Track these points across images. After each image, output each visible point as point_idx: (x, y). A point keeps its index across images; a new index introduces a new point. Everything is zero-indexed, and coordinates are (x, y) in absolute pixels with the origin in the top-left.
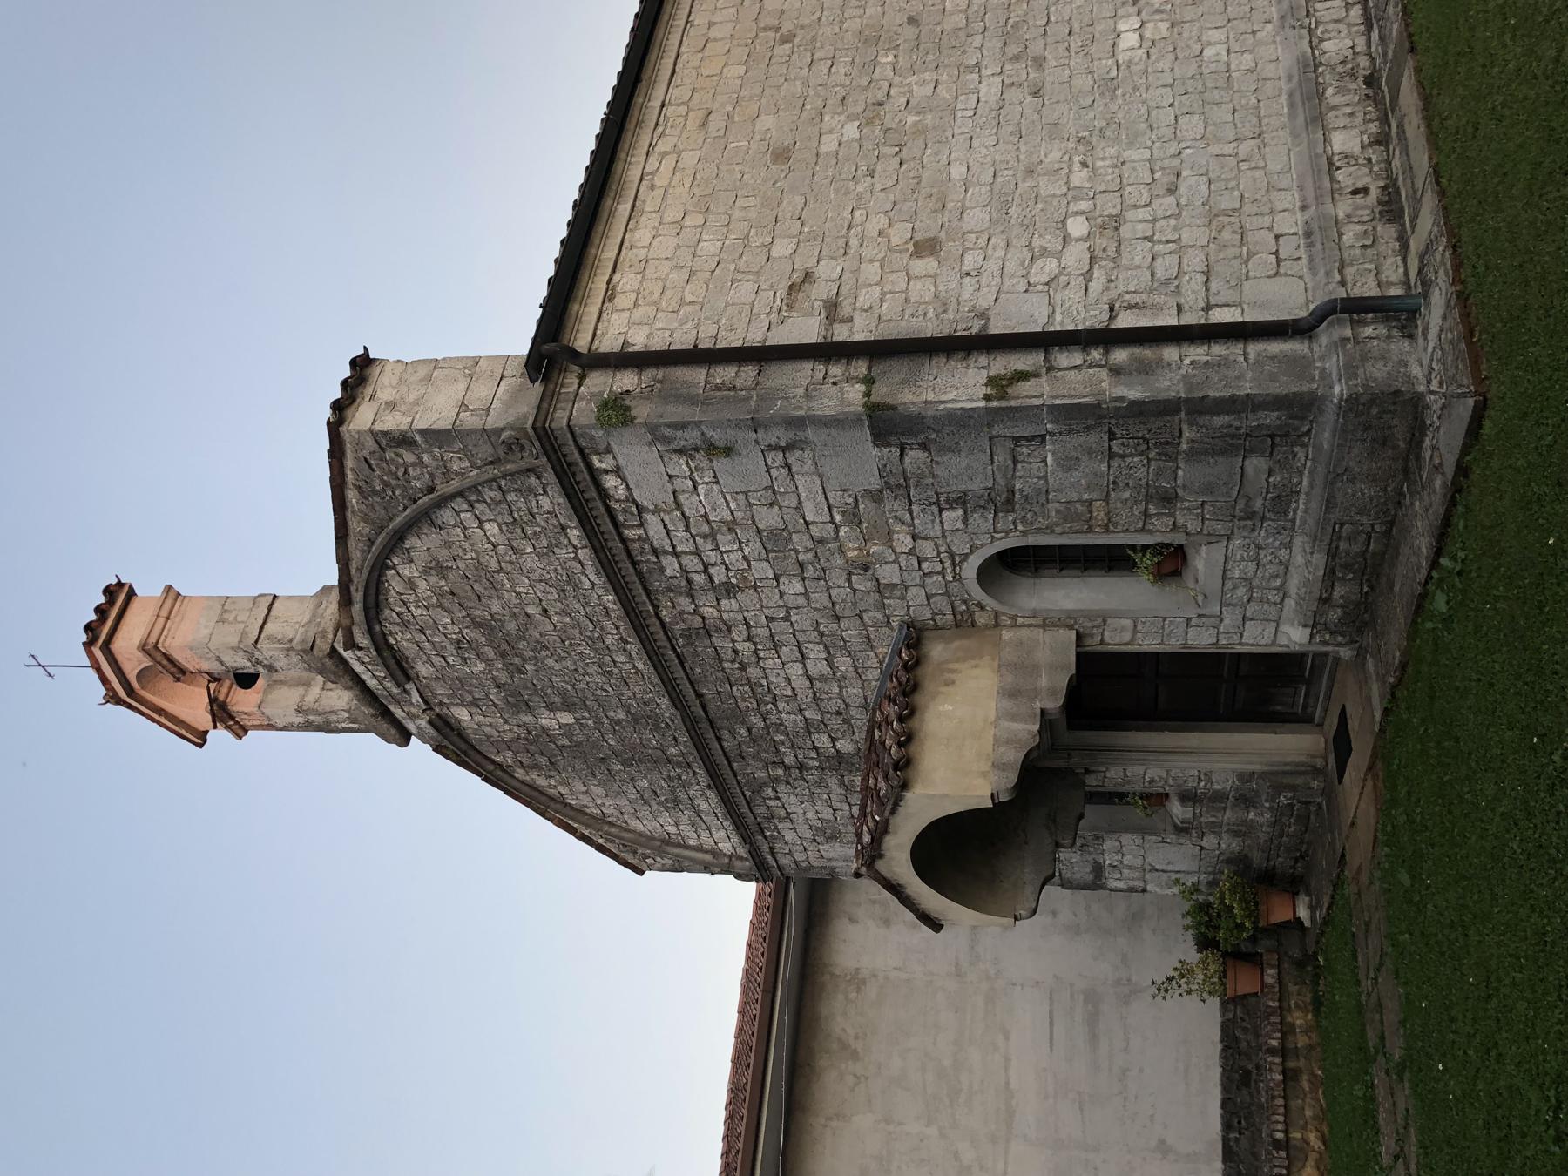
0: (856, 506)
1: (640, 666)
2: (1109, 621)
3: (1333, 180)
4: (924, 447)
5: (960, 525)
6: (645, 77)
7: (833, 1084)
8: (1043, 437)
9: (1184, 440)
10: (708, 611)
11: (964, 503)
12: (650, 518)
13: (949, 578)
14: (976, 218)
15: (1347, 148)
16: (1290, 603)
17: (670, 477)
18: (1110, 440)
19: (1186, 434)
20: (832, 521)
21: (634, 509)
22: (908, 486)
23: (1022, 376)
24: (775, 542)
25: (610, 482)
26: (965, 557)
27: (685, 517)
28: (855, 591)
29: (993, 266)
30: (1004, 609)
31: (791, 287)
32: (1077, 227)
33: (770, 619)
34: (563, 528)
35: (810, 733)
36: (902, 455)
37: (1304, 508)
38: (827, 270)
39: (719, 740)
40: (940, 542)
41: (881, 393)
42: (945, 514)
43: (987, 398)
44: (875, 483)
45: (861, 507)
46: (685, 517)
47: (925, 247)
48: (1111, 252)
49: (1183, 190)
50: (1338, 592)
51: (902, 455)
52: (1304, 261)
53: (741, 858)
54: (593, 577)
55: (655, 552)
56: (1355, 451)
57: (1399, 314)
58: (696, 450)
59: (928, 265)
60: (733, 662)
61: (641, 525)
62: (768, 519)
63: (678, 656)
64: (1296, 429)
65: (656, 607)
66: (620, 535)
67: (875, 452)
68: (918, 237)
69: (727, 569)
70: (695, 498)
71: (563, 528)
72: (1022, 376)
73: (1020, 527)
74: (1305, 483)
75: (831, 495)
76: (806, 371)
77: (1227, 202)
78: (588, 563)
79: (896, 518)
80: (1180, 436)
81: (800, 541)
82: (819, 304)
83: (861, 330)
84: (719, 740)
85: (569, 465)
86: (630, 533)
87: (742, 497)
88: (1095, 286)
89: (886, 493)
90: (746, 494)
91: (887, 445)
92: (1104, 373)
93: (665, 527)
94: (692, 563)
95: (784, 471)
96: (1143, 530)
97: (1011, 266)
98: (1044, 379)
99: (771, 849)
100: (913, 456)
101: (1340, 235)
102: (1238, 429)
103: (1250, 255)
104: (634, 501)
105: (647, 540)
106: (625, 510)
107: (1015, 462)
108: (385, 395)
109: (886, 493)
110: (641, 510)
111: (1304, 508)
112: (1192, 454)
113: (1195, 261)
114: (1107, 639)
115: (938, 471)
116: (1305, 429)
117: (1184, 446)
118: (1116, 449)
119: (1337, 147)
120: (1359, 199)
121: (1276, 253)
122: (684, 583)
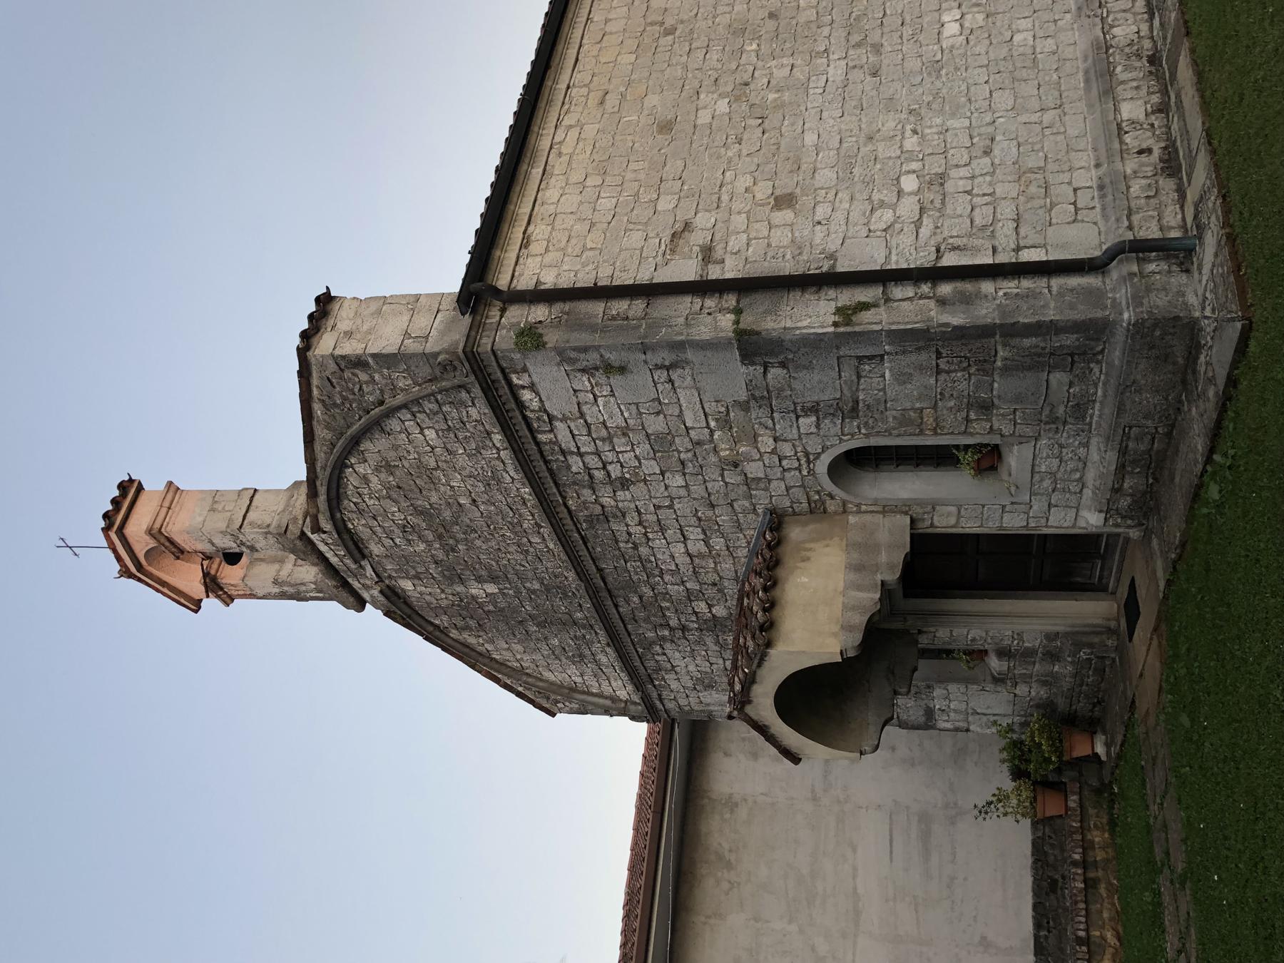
1: (551, 546)
3: (1121, 142)
4: (783, 365)
5: (813, 430)
6: (554, 63)
7: (711, 890)
8: (882, 356)
9: (999, 358)
13: (805, 473)
14: (826, 176)
15: (1134, 116)
16: (1088, 493)
18: (938, 358)
19: (1001, 353)
20: (708, 427)
21: (545, 417)
22: (770, 398)
23: (864, 306)
24: (661, 444)
27: (588, 425)
28: (726, 483)
29: (840, 216)
31: (673, 235)
32: (909, 183)
33: (657, 507)
34: (488, 433)
38: (703, 221)
39: (616, 606)
41: (748, 321)
42: (801, 420)
43: (835, 324)
45: (732, 414)
46: (588, 425)
47: (783, 201)
48: (938, 204)
49: (996, 152)
51: (765, 373)
52: (1098, 209)
53: (635, 703)
54: (512, 473)
55: (563, 452)
57: (1179, 252)
58: (597, 369)
59: (786, 215)
62: (656, 425)
63: (582, 538)
64: (1092, 349)
65: (564, 498)
66: (534, 438)
67: (743, 369)
68: (778, 192)
71: (488, 433)
72: (864, 306)
76: (686, 304)
77: (1033, 161)
78: (508, 462)
80: (996, 355)
82: (696, 249)
83: (731, 270)
84: (616, 606)
85: (493, 382)
87: (634, 407)
88: (925, 231)
90: (637, 404)
91: (753, 364)
92: (932, 304)
94: (593, 462)
95: (668, 386)
97: (854, 216)
98: (882, 308)
99: (660, 695)
101: (1128, 188)
103: (1053, 205)
104: (545, 411)
105: (556, 442)
107: (859, 377)
108: (343, 326)
109: (753, 403)
110: (551, 418)
112: (1006, 370)
113: (1007, 210)
117: (999, 364)
118: (942, 366)
119: (1125, 116)
120: (1144, 158)
121: (1074, 204)
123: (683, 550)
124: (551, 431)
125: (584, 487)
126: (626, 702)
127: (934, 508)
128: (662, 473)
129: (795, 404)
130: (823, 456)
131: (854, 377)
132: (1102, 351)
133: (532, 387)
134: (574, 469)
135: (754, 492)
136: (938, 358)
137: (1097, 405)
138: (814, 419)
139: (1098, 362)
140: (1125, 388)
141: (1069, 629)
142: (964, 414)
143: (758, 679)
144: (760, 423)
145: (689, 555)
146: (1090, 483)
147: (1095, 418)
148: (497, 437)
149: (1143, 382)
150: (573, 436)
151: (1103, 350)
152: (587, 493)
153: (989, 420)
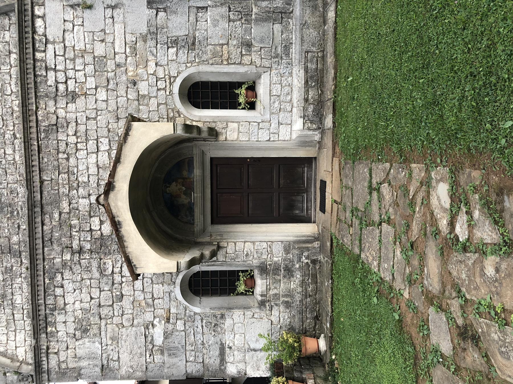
0: (136, 44)
1: (17, 158)
2: (229, 124)
4: (165, 10)
5: (175, 57)
8: (207, 8)
9: (253, 13)
10: (61, 113)
11: (177, 44)
12: (50, 47)
13: (168, 93)
16: (295, 110)
17: (65, 21)
18: (229, 11)
19: (254, 10)
20: (125, 53)
21: (44, 40)
22: (157, 34)
24: (99, 62)
25: (39, 23)
26: (175, 77)
27: (65, 47)
28: (128, 99)
30: (191, 307)
33: (88, 119)
34: (10, 52)
35: (91, 217)
36: (157, 14)
37: (295, 50)
39: (43, 224)
40: (166, 67)
42: (170, 50)
44: (144, 30)
45: (138, 44)
46: (65, 47)
50: (311, 94)
51: (157, 14)
53: (28, 364)
54: (13, 86)
55: (47, 69)
56: (308, 12)
58: (78, 5)
60: (64, 153)
61: (44, 51)
62: (100, 50)
63: (39, 146)
64: (288, 10)
65: (37, 108)
66: (34, 55)
67: (147, 12)
69: (76, 82)
70: (72, 35)
71: (10, 52)
73: (197, 60)
74: (294, 38)
75: (127, 36)
78: (14, 76)
79: (151, 52)
80: (252, 11)
81: (111, 65)
84: (43, 224)
85: (25, 10)
86: (38, 55)
87: (92, 34)
89: (149, 36)
90: (93, 32)
91: (152, 8)
93: (55, 52)
94: (61, 77)
95: (111, 20)
96: (240, 64)
99: (48, 348)
100: (161, 14)
102: (270, 8)
104: (45, 36)
105: (45, 61)
106: (40, 41)
107: (197, 21)
109: (149, 36)
110: (47, 42)
111: (295, 50)
112: (256, 20)
114: (228, 138)
115: (170, 25)
116: (291, 10)
117: (253, 16)
118: (232, 17)
122: (54, 90)
123: (95, 161)
124: (44, 51)
125: (51, 98)
126: (21, 362)
127: (227, 124)
128: (96, 88)
129: (168, 37)
130: (177, 79)
131: (195, 20)
132: (292, 12)
133: (43, 17)
134: (49, 83)
135: (141, 107)
136: (229, 11)
137: (294, 45)
138: (175, 49)
139: (292, 19)
140: (304, 25)
141: (295, 238)
142: (240, 50)
143: (121, 160)
144: (151, 52)
145: (98, 166)
146: (295, 105)
147: (293, 55)
148: (14, 56)
149: (309, 21)
150: (55, 55)
151: (293, 10)
152: (51, 103)
153: (250, 55)
